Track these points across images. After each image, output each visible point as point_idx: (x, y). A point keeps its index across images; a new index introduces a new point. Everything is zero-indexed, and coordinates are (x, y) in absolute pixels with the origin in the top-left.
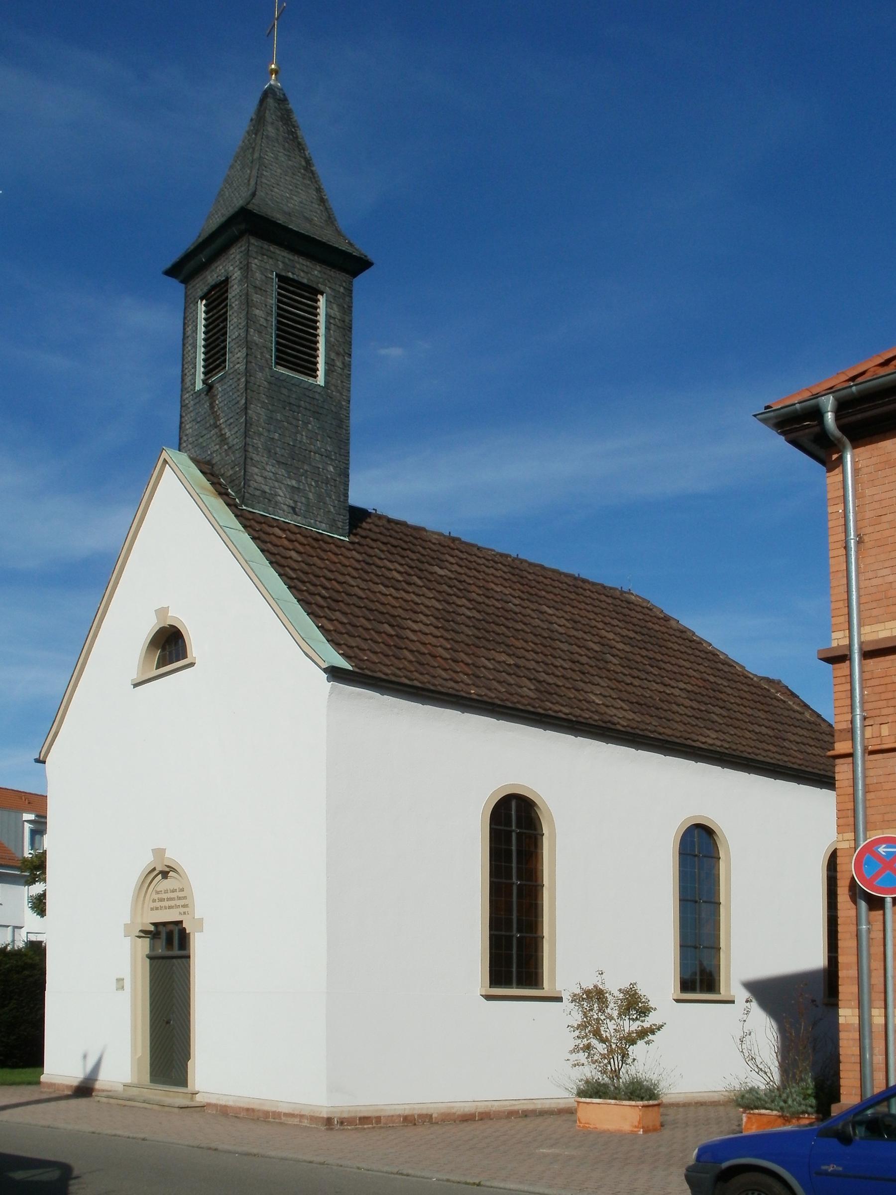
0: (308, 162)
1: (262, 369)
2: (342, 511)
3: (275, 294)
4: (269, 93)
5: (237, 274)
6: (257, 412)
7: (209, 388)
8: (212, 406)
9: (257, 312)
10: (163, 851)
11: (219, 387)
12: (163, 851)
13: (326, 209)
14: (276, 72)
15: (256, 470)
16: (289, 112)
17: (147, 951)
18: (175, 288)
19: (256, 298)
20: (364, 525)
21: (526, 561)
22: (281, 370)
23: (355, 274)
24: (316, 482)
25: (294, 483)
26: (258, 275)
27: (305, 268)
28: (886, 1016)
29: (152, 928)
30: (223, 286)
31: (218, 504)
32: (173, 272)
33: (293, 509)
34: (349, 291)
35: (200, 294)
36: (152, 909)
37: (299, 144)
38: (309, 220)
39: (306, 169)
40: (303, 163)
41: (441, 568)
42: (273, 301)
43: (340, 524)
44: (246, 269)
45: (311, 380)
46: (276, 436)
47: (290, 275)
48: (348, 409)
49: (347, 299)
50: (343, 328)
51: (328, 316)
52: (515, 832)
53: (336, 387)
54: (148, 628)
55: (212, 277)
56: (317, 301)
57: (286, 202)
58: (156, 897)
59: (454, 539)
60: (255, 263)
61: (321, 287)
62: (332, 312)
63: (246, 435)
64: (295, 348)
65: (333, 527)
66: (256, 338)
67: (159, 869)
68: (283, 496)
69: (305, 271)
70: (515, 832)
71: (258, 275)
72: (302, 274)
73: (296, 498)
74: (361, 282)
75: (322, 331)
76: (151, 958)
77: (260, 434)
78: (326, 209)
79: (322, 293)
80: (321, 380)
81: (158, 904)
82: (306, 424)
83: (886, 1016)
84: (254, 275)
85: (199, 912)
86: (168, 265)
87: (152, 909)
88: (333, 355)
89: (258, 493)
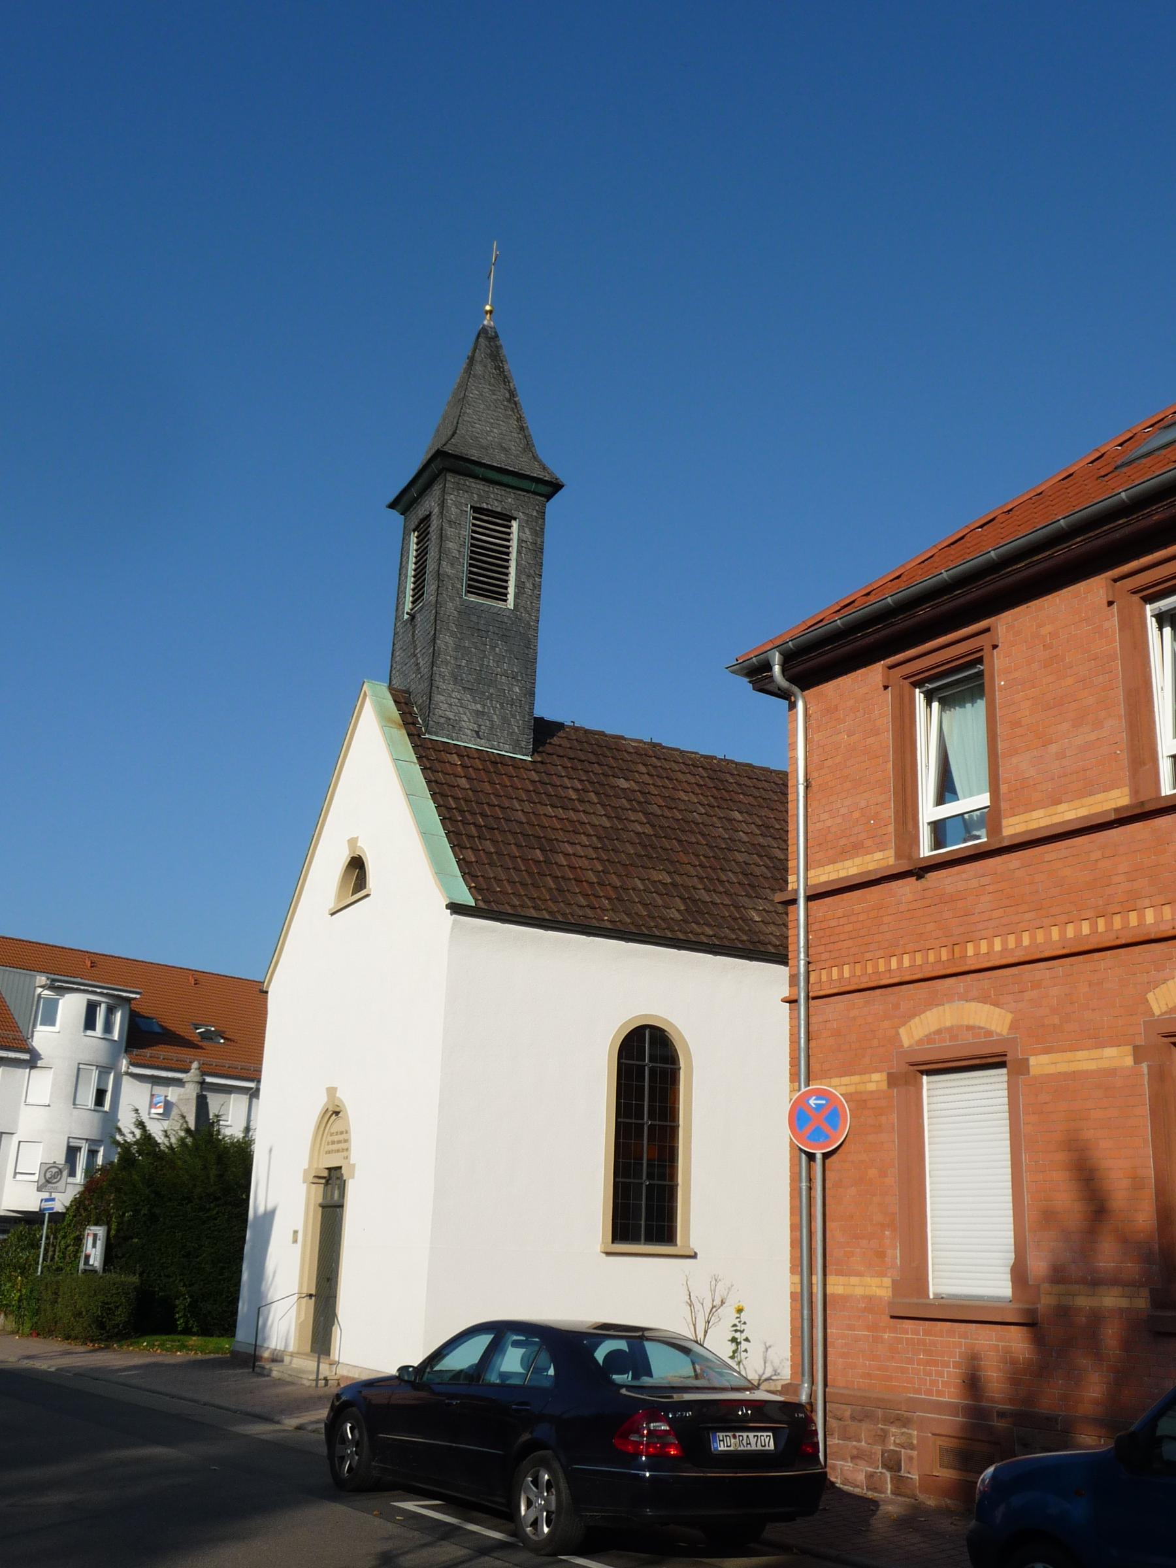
0: (512, 394)
1: (452, 599)
2: (527, 731)
3: (469, 527)
4: (484, 331)
5: (436, 510)
6: (446, 641)
7: (413, 617)
8: (413, 636)
9: (451, 545)
10: (335, 1089)
11: (419, 618)
12: (335, 1089)
13: (525, 437)
14: (491, 312)
15: (442, 698)
16: (499, 347)
17: (320, 1200)
18: (396, 517)
19: (450, 531)
20: (555, 740)
21: (732, 762)
22: (472, 598)
23: (549, 497)
24: (501, 704)
25: (479, 707)
26: (454, 510)
27: (499, 498)
28: (825, 1285)
29: (325, 1174)
30: (427, 518)
31: (401, 735)
32: (392, 506)
33: (477, 733)
34: (542, 514)
35: (413, 526)
36: (328, 1152)
37: (505, 377)
38: (505, 450)
39: (509, 401)
40: (507, 395)
41: (627, 780)
42: (466, 533)
43: (523, 744)
44: (442, 504)
45: (501, 604)
46: (464, 663)
47: (485, 506)
48: (536, 630)
49: (540, 521)
50: (535, 550)
51: (520, 540)
52: (648, 1071)
53: (525, 608)
54: (343, 859)
55: (421, 512)
56: (510, 527)
57: (487, 437)
58: (330, 1139)
59: (655, 745)
60: (450, 499)
61: (515, 513)
62: (524, 537)
63: (433, 664)
64: (486, 574)
65: (517, 747)
66: (449, 570)
67: (331, 1109)
68: (468, 723)
69: (497, 499)
70: (648, 1071)
71: (454, 510)
72: (496, 503)
73: (480, 721)
74: (554, 506)
75: (513, 555)
76: (323, 1206)
77: (447, 663)
78: (525, 437)
79: (515, 519)
80: (510, 604)
81: (331, 1147)
82: (493, 648)
83: (825, 1285)
84: (455, 503)
85: (353, 1159)
86: (391, 498)
87: (328, 1152)
88: (523, 578)
89: (442, 720)
